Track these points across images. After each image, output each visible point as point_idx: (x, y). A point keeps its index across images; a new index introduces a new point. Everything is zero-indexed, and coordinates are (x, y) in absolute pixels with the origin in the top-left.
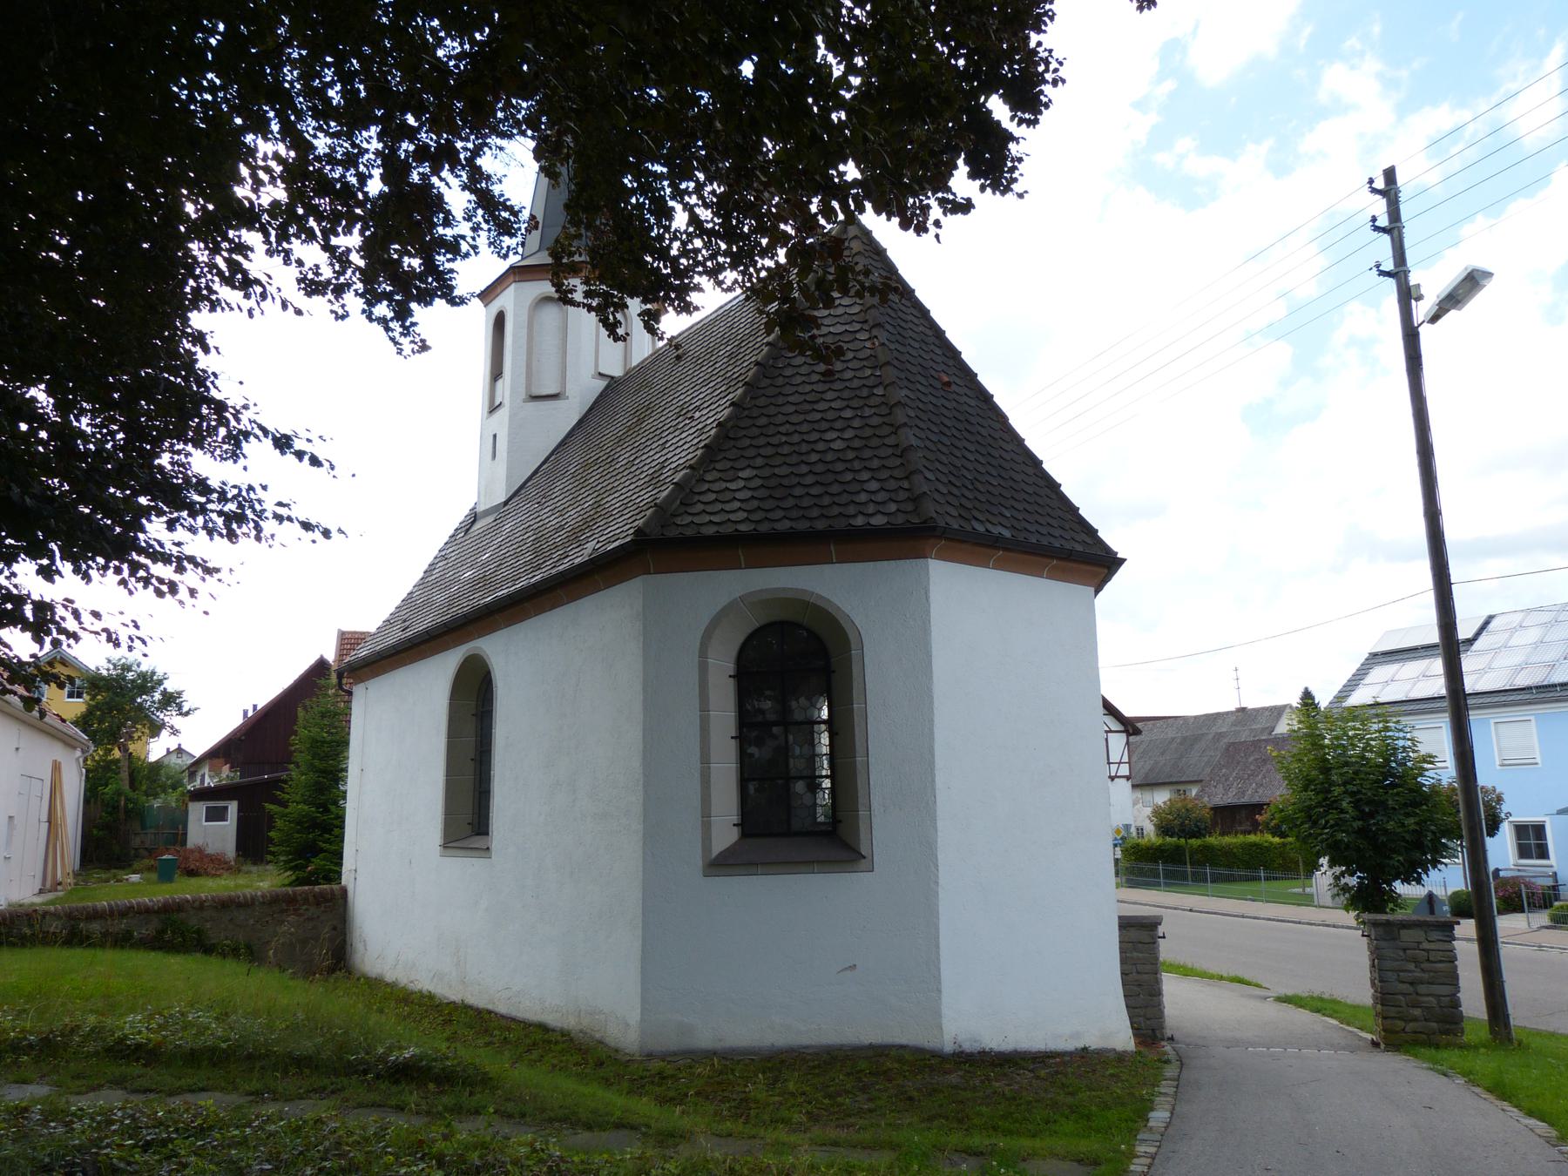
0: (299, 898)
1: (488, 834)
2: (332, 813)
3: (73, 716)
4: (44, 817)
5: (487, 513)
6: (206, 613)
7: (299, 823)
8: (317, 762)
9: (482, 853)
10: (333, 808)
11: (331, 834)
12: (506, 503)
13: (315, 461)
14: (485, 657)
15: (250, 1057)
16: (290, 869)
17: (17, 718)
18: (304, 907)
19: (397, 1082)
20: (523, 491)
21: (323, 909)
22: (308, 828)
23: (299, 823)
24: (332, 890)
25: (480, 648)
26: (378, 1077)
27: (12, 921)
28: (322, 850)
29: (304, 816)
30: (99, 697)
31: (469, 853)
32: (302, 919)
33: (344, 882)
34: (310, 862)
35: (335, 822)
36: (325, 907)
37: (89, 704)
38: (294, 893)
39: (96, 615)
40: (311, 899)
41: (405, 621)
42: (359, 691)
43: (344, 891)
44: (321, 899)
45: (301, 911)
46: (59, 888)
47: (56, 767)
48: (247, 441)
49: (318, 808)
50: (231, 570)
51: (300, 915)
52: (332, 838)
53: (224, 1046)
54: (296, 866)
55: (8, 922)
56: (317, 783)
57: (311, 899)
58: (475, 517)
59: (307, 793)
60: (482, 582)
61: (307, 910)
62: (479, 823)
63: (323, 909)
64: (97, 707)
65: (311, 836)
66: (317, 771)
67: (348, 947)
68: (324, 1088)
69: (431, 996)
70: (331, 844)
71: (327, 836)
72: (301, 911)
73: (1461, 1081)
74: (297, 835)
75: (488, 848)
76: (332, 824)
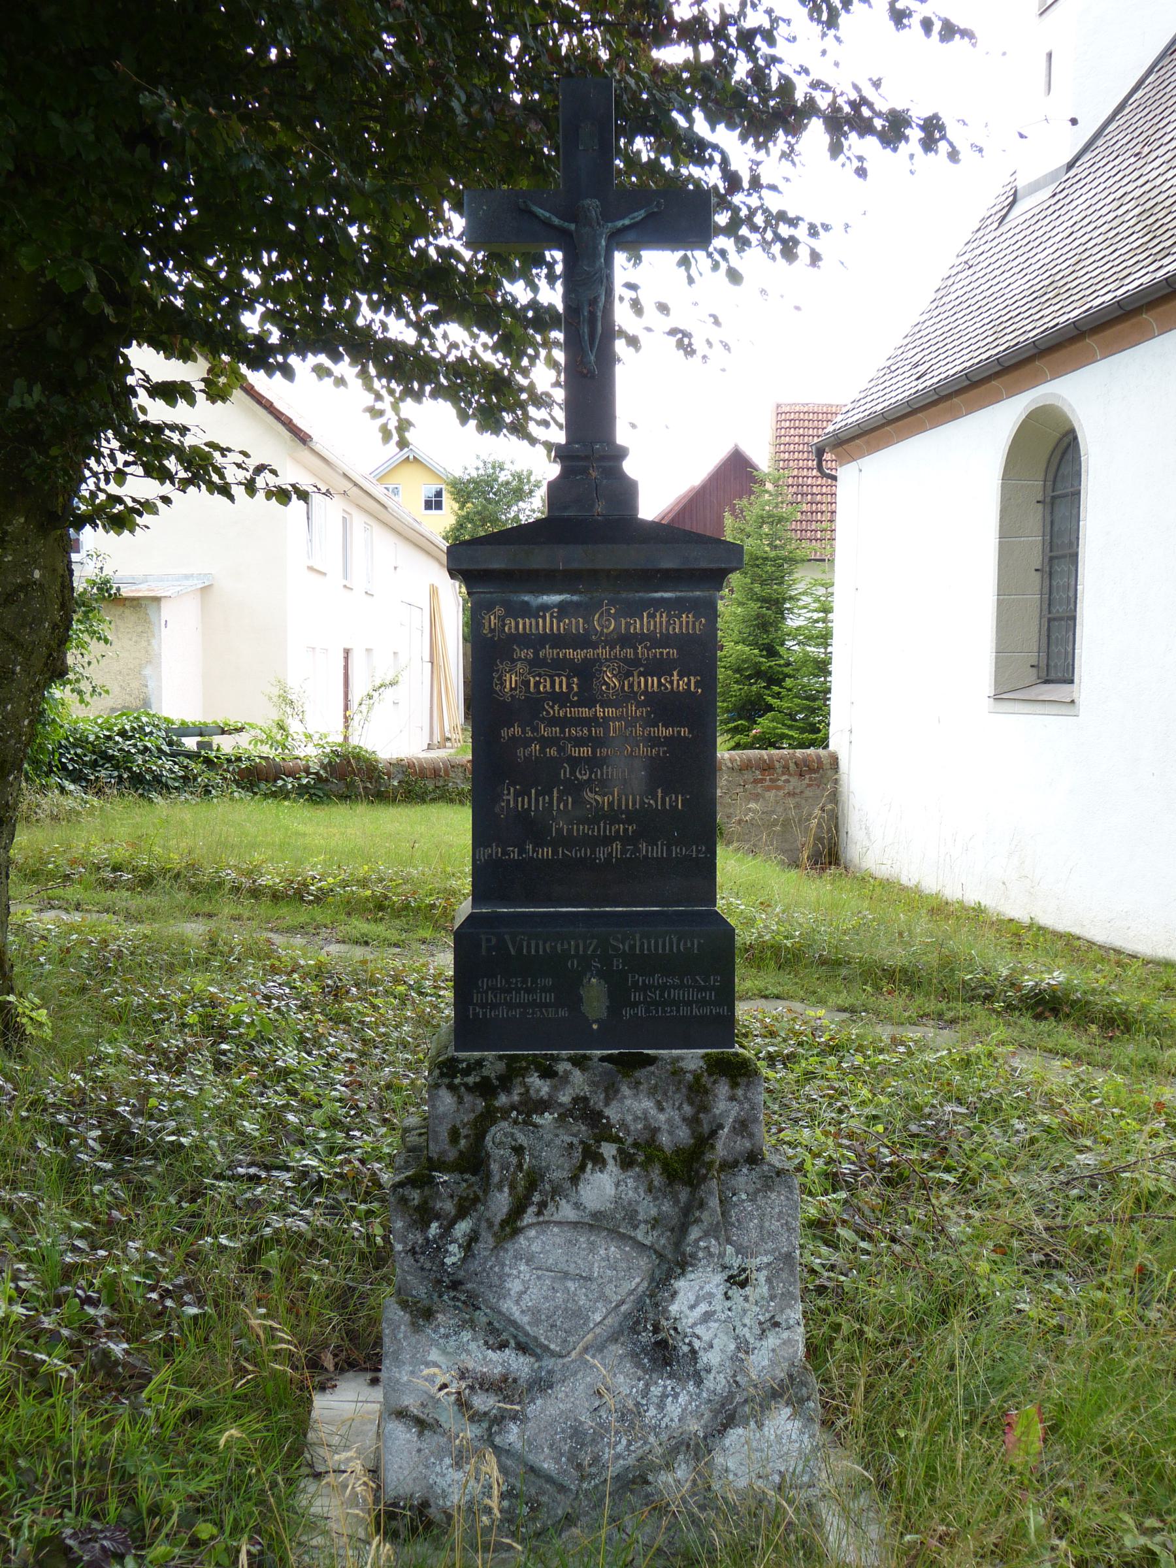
0: (777, 765)
1: (1072, 682)
2: (781, 657)
3: (442, 530)
4: (427, 657)
5: (1035, 187)
6: (797, 308)
7: (738, 670)
8: (757, 588)
9: (1064, 709)
10: (782, 650)
11: (782, 687)
12: (1070, 166)
13: (949, 31)
14: (1066, 409)
15: (823, 962)
16: (728, 731)
17: (399, 534)
18: (784, 778)
19: (1038, 1017)
20: (1100, 142)
21: (807, 781)
22: (749, 677)
23: (738, 670)
24: (819, 757)
25: (1059, 397)
26: (1010, 1007)
27: (447, 773)
28: (770, 708)
29: (744, 661)
30: (469, 505)
31: (1038, 708)
32: (781, 793)
33: (832, 748)
34: (755, 722)
35: (786, 670)
36: (810, 779)
37: (457, 514)
38: (771, 758)
39: (663, 308)
40: (792, 766)
41: (916, 365)
42: (848, 474)
43: (835, 761)
44: (805, 769)
45: (780, 783)
46: (448, 744)
47: (434, 592)
48: (848, 11)
49: (761, 651)
50: (847, 226)
51: (779, 788)
52: (784, 692)
53: (789, 943)
54: (736, 728)
55: (442, 773)
56: (758, 616)
57: (792, 766)
58: (1015, 194)
59: (748, 630)
60: (1041, 296)
61: (787, 781)
62: (1048, 665)
63: (807, 781)
64: (467, 518)
65: (754, 688)
66: (758, 600)
67: (842, 834)
68: (940, 1015)
69: (979, 910)
70: (781, 699)
71: (776, 689)
72: (780, 783)
73: (455, 1099)
74: (736, 687)
75: (1073, 702)
76: (782, 672)
